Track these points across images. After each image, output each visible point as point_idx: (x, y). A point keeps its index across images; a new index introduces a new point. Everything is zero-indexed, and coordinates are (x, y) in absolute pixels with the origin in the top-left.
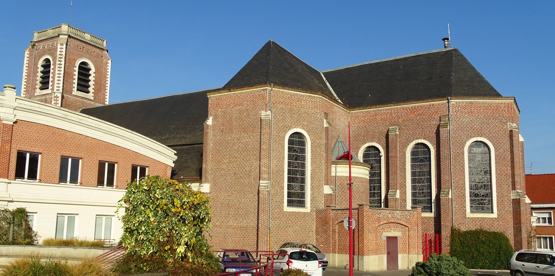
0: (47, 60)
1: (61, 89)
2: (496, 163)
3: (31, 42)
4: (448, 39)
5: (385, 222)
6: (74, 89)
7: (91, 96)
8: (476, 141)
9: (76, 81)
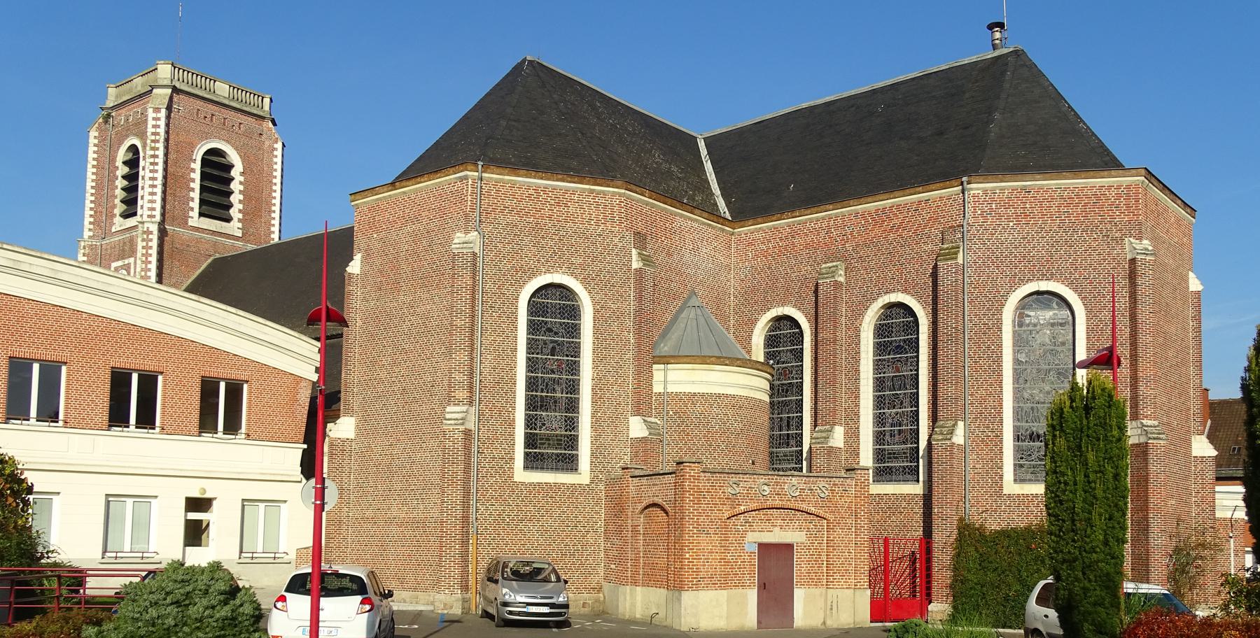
0: (133, 149)
1: (158, 213)
3: (102, 109)
4: (1001, 25)
5: (754, 505)
6: (191, 214)
7: (234, 227)
8: (1038, 293)
9: (196, 195)
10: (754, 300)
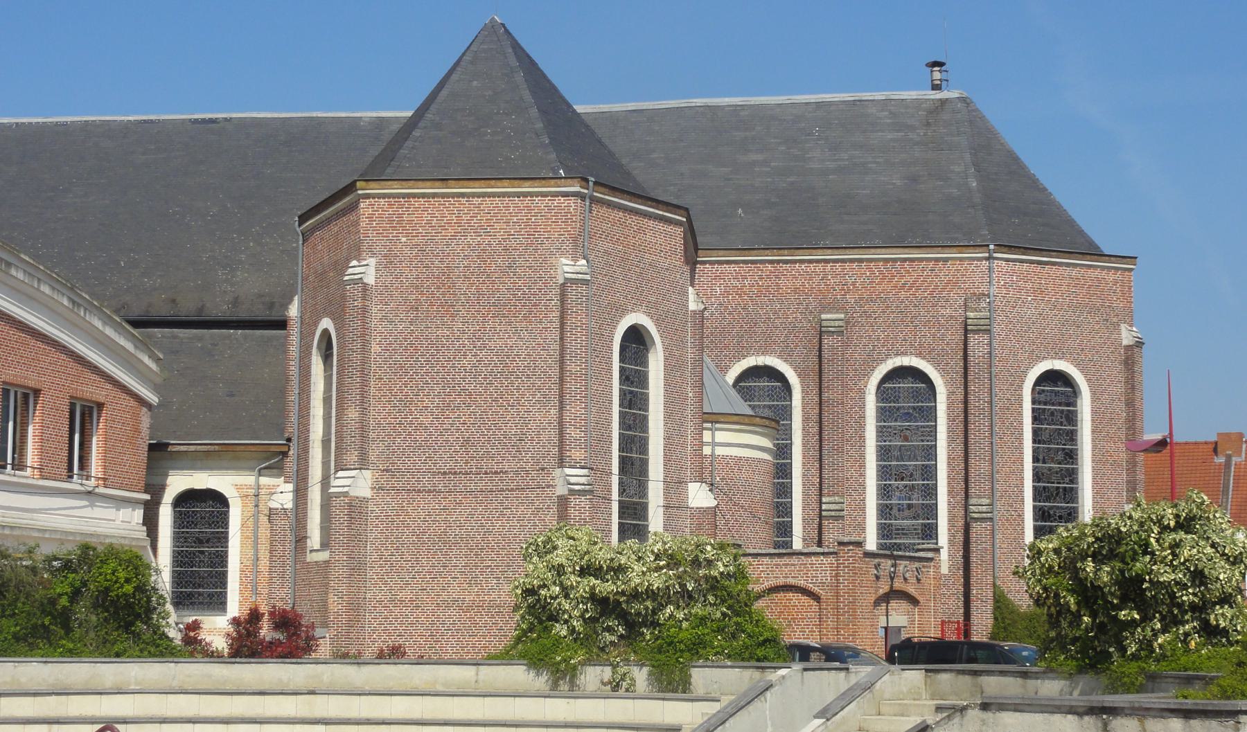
2: (1093, 432)
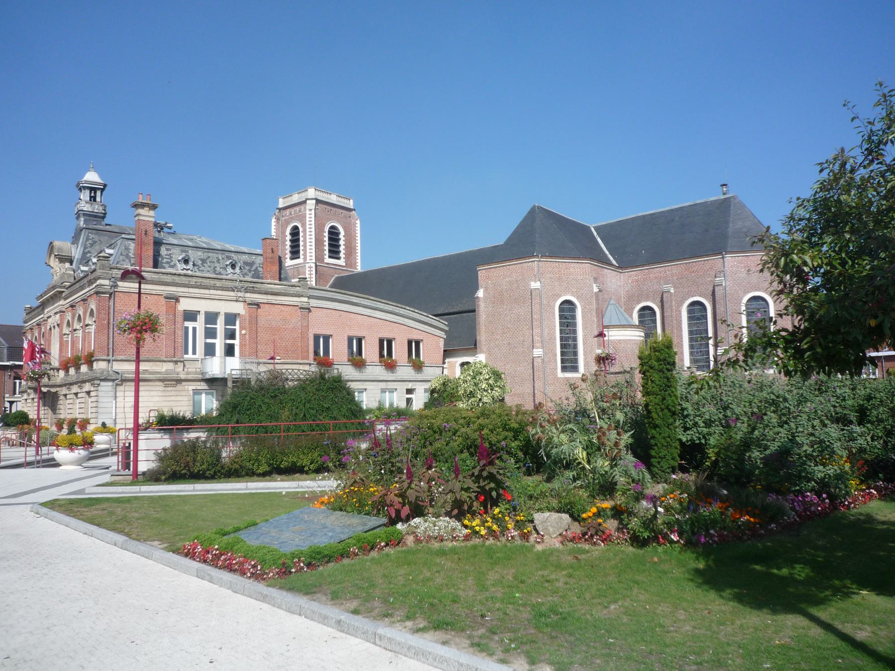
1: (314, 258)
7: (342, 262)
10: (631, 299)
